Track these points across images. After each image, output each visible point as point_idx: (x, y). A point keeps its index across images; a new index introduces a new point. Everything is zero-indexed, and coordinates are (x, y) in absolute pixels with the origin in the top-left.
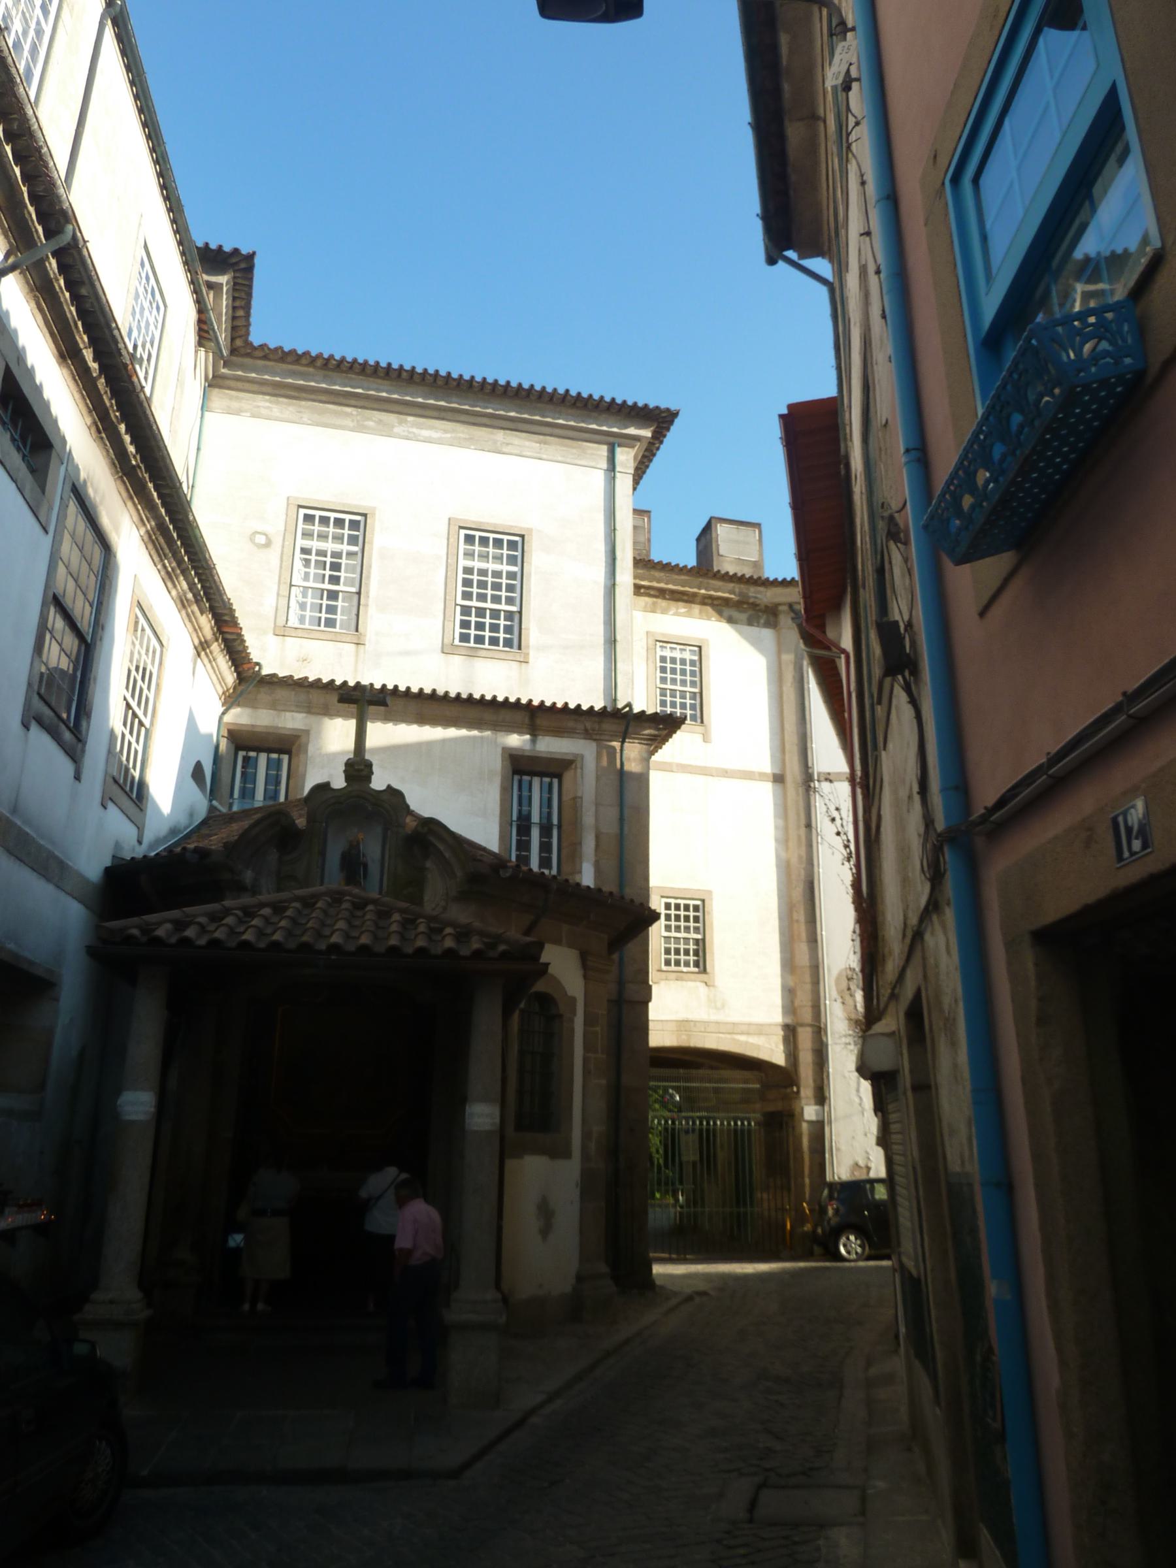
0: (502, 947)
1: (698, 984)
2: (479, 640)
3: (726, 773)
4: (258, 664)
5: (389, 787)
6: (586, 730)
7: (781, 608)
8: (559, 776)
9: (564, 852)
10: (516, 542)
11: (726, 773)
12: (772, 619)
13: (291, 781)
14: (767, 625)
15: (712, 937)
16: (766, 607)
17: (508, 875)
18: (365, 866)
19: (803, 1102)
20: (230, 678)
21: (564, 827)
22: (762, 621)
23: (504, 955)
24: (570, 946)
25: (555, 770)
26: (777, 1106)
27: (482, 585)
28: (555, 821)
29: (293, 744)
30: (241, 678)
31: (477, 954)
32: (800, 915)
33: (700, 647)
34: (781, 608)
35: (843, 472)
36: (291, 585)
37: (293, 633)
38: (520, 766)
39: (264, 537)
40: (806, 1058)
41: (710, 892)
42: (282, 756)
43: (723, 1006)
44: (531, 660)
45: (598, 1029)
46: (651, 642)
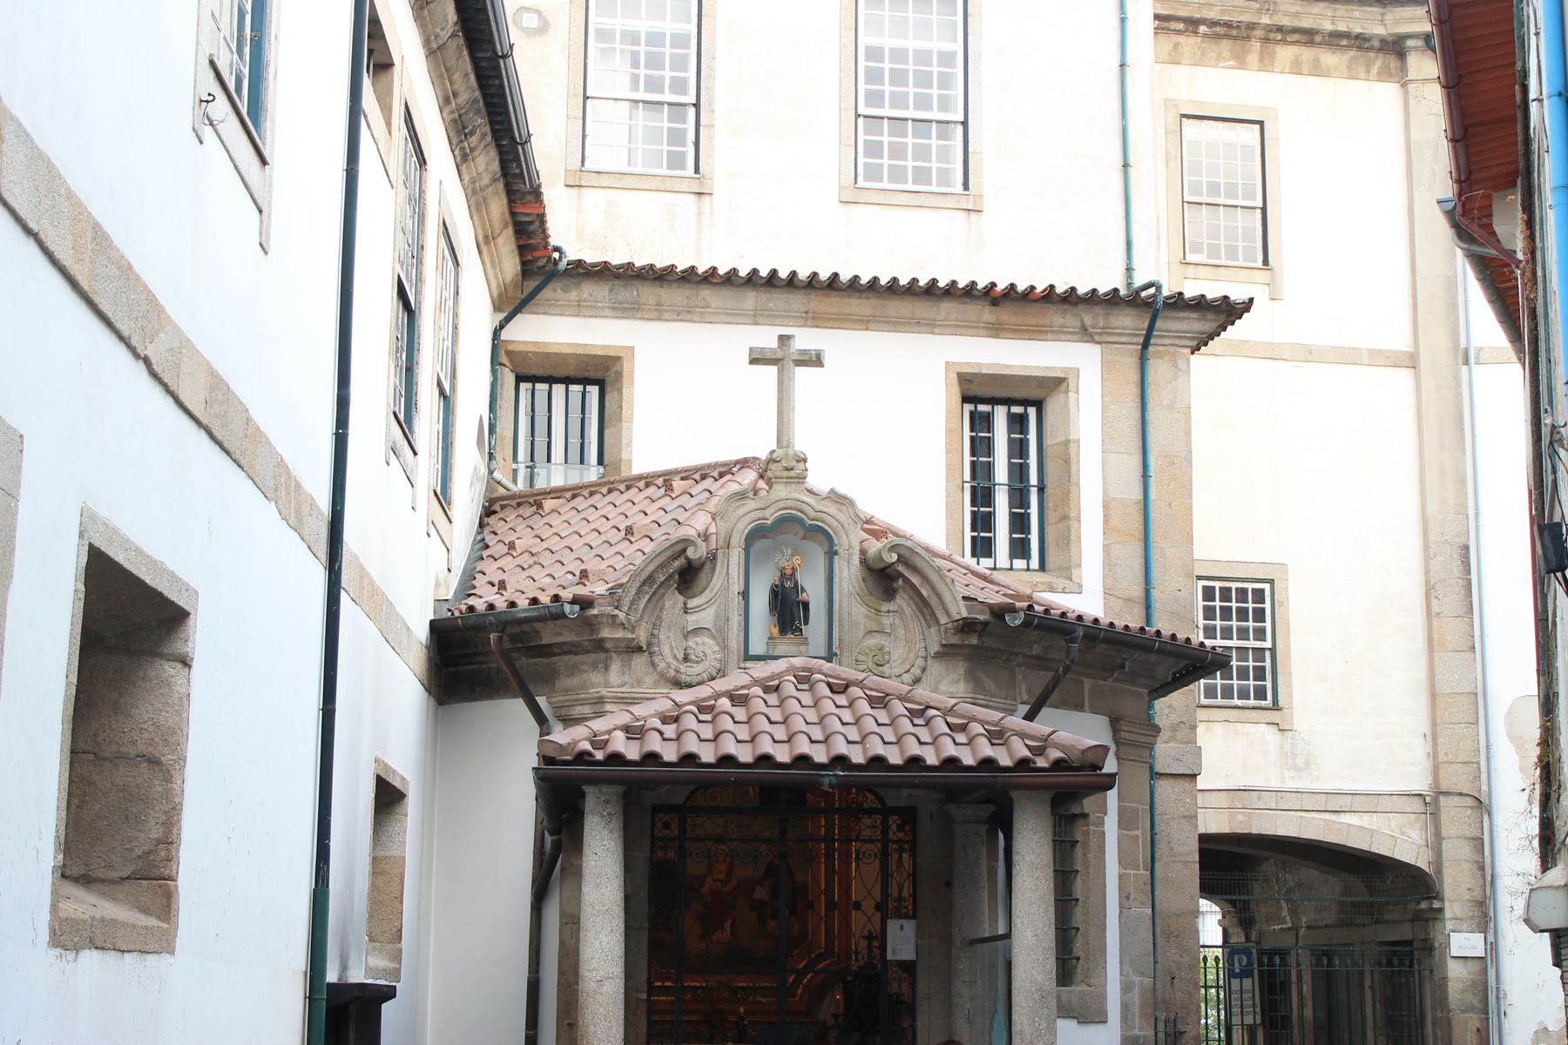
0: (1055, 754)
1: (1263, 727)
2: (897, 174)
3: (1308, 354)
4: (557, 249)
5: (832, 490)
6: (1084, 329)
7: (1410, 43)
8: (1039, 404)
9: (1051, 532)
10: (1263, 591)
11: (1308, 354)
12: (1393, 63)
13: (607, 432)
14: (1385, 75)
15: (1288, 646)
16: (1383, 41)
17: (1018, 622)
18: (806, 605)
19: (1449, 925)
20: (511, 266)
21: (1049, 491)
22: (1375, 70)
23: (1058, 765)
24: (1095, 711)
25: (1028, 400)
26: (1404, 932)
27: (899, 77)
28: (1034, 480)
29: (607, 369)
30: (527, 269)
31: (1023, 764)
32: (1449, 602)
33: (1261, 123)
34: (1410, 43)
35: (1518, 98)
36: (586, 98)
37: (594, 180)
38: (978, 396)
39: (535, 16)
40: (1457, 854)
41: (1283, 566)
42: (589, 388)
43: (1308, 765)
44: (986, 206)
45: (1139, 832)
46: (1173, 120)
